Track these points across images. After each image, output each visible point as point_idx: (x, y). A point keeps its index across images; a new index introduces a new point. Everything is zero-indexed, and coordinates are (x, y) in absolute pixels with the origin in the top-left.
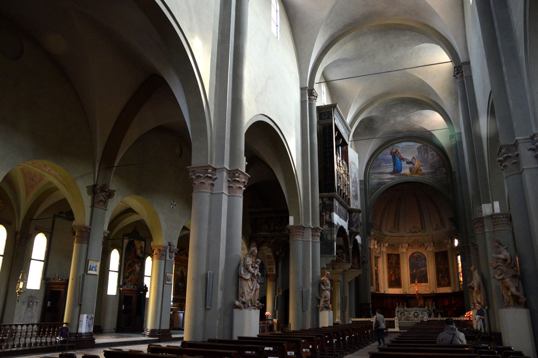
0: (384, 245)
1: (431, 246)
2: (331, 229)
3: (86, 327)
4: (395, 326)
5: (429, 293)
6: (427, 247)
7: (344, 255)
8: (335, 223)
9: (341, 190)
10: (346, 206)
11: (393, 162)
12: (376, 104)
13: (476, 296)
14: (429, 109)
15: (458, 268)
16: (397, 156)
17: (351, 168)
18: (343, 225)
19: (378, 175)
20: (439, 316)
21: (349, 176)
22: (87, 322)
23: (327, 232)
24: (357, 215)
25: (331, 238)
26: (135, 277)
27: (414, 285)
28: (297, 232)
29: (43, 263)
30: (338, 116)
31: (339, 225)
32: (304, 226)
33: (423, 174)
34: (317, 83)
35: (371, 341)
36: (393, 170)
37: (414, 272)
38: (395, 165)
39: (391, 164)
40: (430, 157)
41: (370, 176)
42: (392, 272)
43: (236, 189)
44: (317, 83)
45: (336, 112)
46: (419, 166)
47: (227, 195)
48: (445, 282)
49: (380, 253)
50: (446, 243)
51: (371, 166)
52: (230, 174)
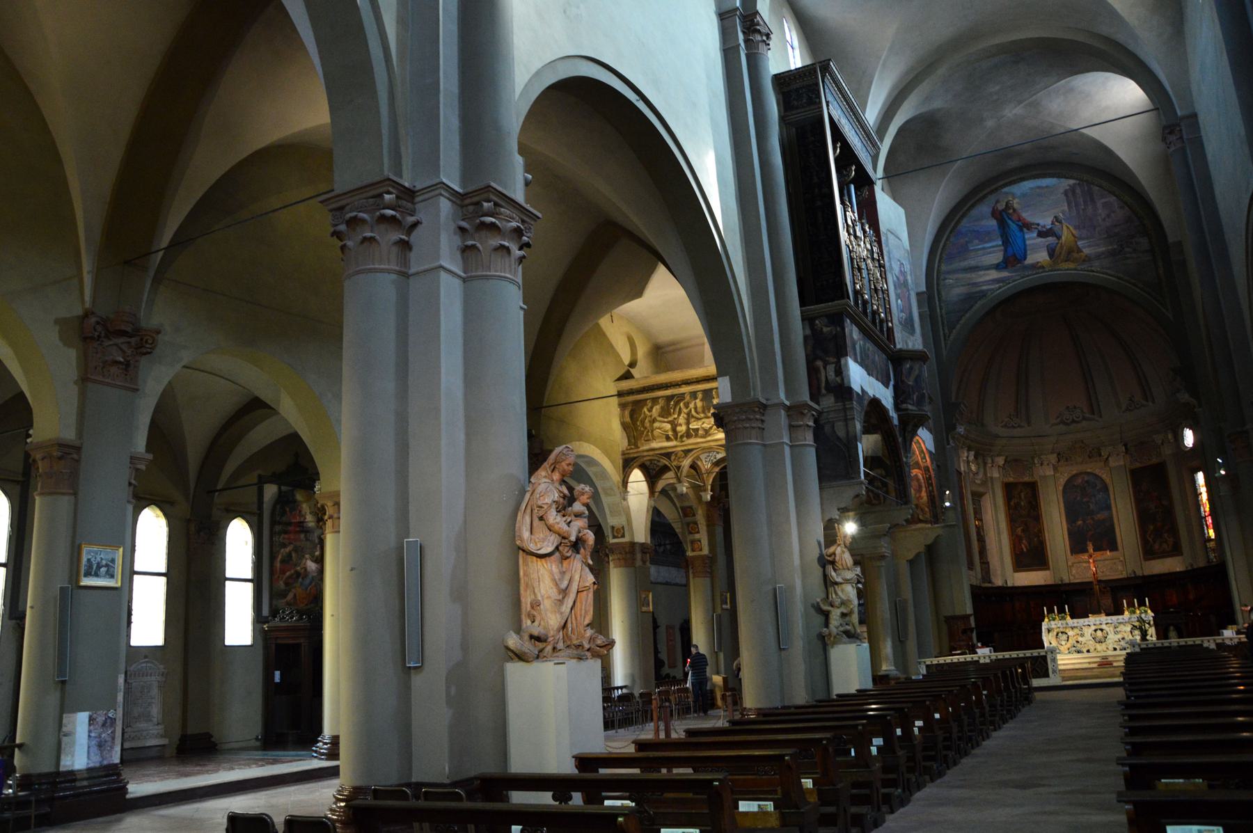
0: (993, 462)
1: (1118, 455)
2: (844, 405)
3: (88, 752)
4: (1047, 669)
5: (1124, 575)
6: (1108, 457)
7: (891, 483)
8: (856, 387)
9: (865, 302)
10: (886, 345)
11: (1002, 236)
12: (942, 71)
15: (1198, 504)
16: (1010, 219)
17: (887, 246)
20: (1172, 633)
21: (884, 267)
22: (93, 735)
24: (917, 367)
26: (308, 592)
27: (1085, 557)
28: (743, 420)
29: (250, 585)
30: (837, 98)
31: (867, 393)
33: (1088, 259)
35: (992, 723)
36: (1004, 257)
37: (1080, 525)
38: (1006, 242)
39: (994, 243)
40: (1102, 212)
42: (1019, 529)
45: (830, 86)
46: (1073, 238)
47: (459, 276)
48: (1165, 546)
49: (984, 483)
51: (941, 254)
52: (467, 206)
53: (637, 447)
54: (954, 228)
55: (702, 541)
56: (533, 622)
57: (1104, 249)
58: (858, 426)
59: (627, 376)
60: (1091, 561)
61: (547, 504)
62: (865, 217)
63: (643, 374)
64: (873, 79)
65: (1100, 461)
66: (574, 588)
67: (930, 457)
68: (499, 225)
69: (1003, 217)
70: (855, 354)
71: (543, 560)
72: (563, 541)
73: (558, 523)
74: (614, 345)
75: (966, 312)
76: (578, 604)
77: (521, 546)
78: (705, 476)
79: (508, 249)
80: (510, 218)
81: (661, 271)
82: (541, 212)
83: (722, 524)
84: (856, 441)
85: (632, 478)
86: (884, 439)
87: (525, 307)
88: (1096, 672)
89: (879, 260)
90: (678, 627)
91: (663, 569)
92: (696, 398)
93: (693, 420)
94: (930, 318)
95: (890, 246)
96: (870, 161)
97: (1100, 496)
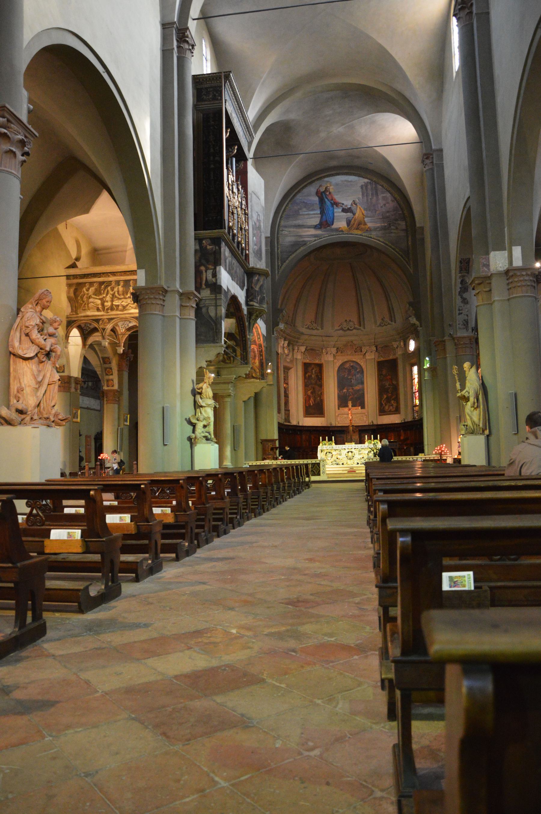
0: (298, 349)
1: (371, 352)
8: (224, 286)
9: (234, 235)
11: (320, 208)
12: (298, 94)
13: (470, 413)
14: (389, 112)
15: (412, 385)
17: (251, 202)
18: (236, 294)
19: (295, 229)
21: (247, 215)
23: (207, 302)
25: (216, 314)
32: (166, 288)
33: (369, 230)
34: (194, 19)
37: (345, 392)
38: (322, 213)
40: (381, 202)
41: (281, 231)
43: (2, 155)
44: (194, 19)
45: (228, 89)
46: (362, 216)
48: (391, 408)
49: (292, 361)
50: (395, 346)
53: (77, 314)
54: (292, 199)
55: (114, 381)
56: (18, 401)
57: (379, 225)
58: (223, 311)
59: (73, 266)
60: (350, 412)
61: (32, 325)
62: (239, 180)
63: (84, 266)
64: (256, 90)
65: (361, 355)
66: (46, 381)
67: (263, 338)
68: (10, 135)
69: (322, 196)
70: (226, 266)
71: (27, 362)
72: (41, 351)
73: (38, 339)
74: (67, 244)
75: (293, 253)
76: (48, 392)
77: (12, 351)
78: (120, 337)
79: (14, 153)
80: (17, 132)
81: (105, 196)
82: (38, 133)
83: (127, 370)
84: (221, 319)
85: (71, 334)
86: (237, 322)
87: (22, 197)
88: (346, 475)
89: (245, 210)
90: (93, 437)
91: (86, 398)
92: (119, 285)
93: (116, 299)
94: (271, 254)
95: (253, 202)
96: (247, 145)
97: (358, 376)
